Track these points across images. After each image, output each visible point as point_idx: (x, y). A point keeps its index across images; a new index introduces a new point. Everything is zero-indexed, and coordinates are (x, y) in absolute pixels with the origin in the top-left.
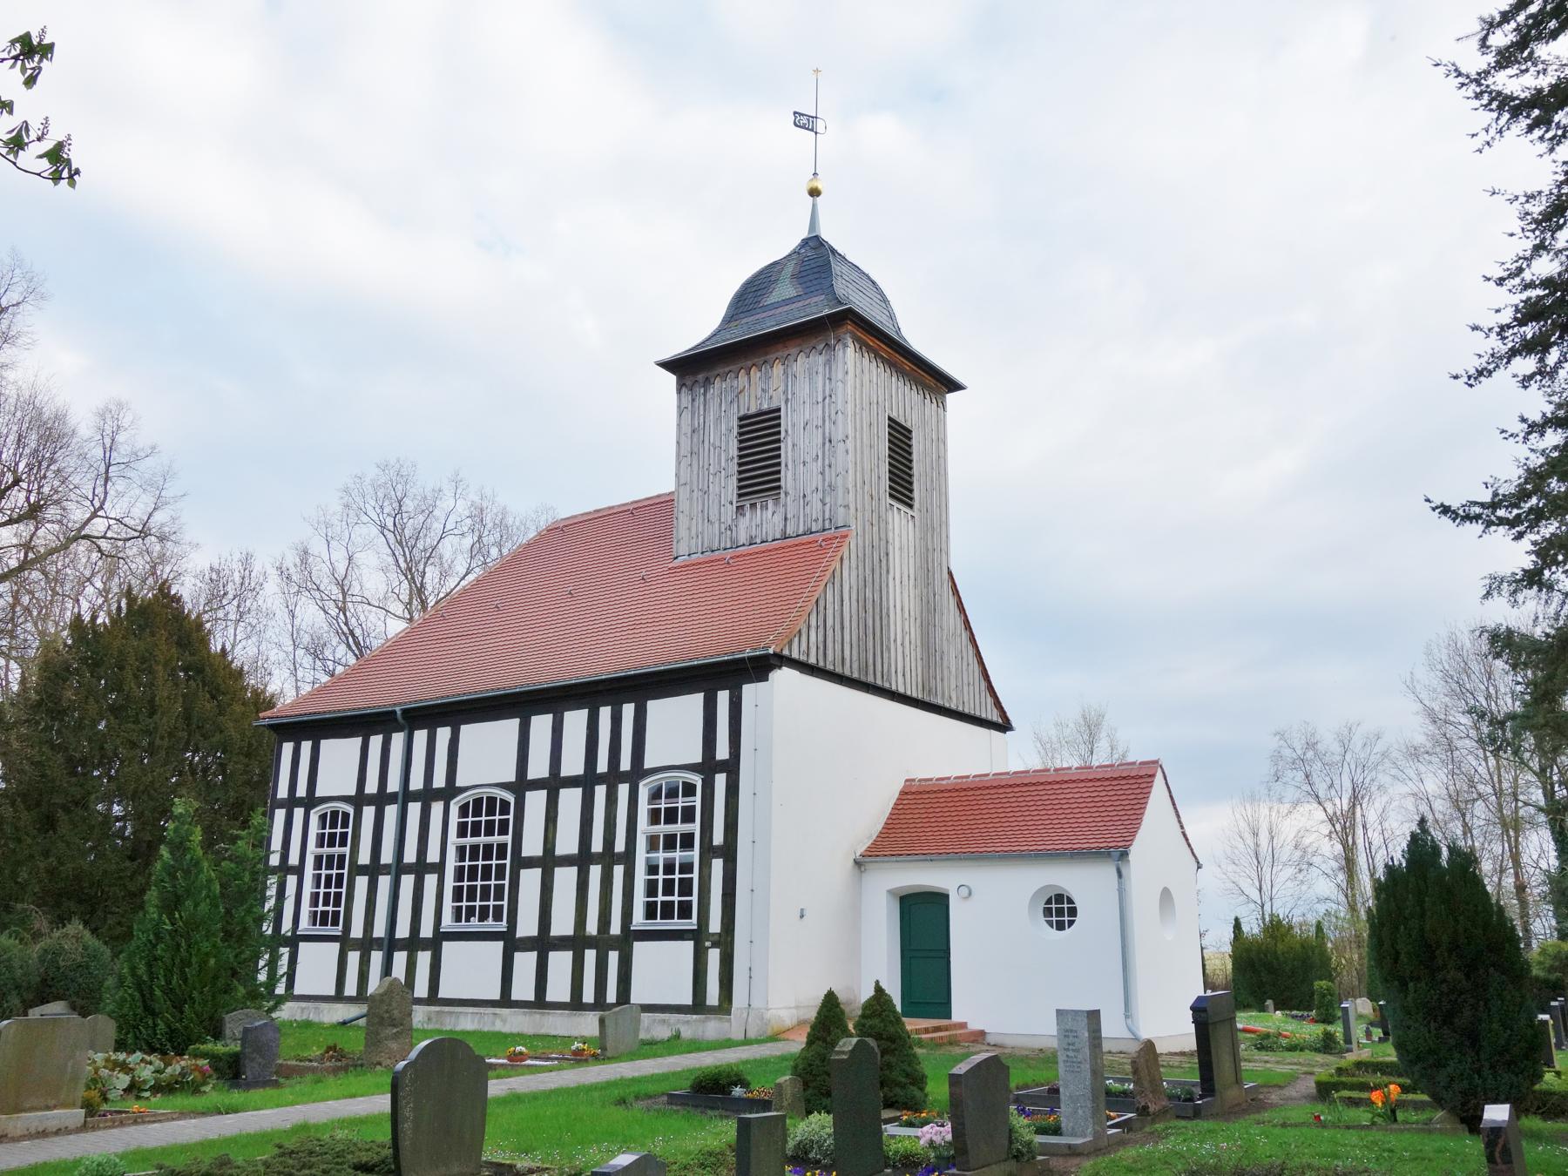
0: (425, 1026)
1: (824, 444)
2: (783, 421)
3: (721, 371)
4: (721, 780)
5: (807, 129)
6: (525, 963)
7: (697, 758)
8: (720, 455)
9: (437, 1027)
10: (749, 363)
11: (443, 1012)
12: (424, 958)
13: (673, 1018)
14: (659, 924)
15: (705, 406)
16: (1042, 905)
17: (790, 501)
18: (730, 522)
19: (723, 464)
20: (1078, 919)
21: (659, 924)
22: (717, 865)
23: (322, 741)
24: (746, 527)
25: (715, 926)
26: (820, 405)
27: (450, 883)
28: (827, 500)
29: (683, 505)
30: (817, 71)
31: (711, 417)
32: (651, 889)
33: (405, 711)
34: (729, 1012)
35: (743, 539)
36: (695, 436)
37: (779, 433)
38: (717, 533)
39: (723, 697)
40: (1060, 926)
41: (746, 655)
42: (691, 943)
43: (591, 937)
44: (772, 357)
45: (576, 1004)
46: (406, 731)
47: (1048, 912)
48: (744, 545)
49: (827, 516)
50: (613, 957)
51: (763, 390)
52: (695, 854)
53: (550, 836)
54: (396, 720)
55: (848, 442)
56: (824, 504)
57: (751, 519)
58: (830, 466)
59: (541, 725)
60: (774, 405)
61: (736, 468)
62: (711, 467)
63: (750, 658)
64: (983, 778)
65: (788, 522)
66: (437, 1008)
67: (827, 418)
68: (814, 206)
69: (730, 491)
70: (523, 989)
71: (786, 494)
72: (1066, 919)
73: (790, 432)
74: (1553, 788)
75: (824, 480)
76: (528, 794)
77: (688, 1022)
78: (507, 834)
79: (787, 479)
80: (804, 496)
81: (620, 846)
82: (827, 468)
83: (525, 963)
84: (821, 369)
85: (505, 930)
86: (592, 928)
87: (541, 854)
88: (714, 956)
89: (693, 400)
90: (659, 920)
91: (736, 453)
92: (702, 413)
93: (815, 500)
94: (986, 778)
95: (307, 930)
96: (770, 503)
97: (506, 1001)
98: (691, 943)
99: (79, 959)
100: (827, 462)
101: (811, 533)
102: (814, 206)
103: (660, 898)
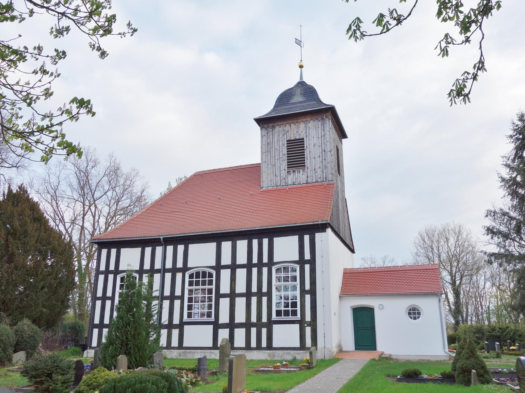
0: (178, 357)
1: (322, 152)
2: (305, 143)
3: (279, 124)
4: (307, 267)
5: (299, 45)
7: (214, 264)
8: (279, 153)
9: (184, 358)
10: (291, 122)
11: (187, 352)
12: (175, 332)
13: (292, 352)
14: (283, 318)
15: (272, 135)
16: (408, 312)
17: (309, 171)
18: (284, 176)
19: (281, 156)
21: (283, 318)
22: (308, 297)
23: (121, 249)
24: (291, 179)
25: (308, 318)
26: (320, 139)
27: (186, 303)
28: (324, 171)
29: (264, 168)
30: (301, 26)
31: (276, 139)
33: (164, 238)
35: (290, 182)
36: (269, 146)
37: (304, 147)
38: (279, 180)
39: (307, 238)
41: (319, 223)
42: (298, 325)
43: (254, 323)
44: (299, 120)
45: (259, 347)
46: (164, 246)
47: (409, 314)
48: (290, 185)
49: (324, 177)
50: (264, 331)
51: (296, 132)
52: (298, 293)
54: (160, 241)
55: (332, 152)
57: (293, 176)
58: (325, 160)
60: (301, 137)
61: (286, 158)
62: (276, 157)
63: (321, 224)
64: (374, 269)
65: (309, 178)
66: (183, 351)
67: (323, 143)
68: (301, 71)
69: (284, 166)
71: (307, 168)
73: (308, 147)
74: (94, 283)
75: (323, 164)
76: (222, 271)
77: (299, 353)
78: (212, 285)
79: (307, 163)
80: (315, 169)
81: (265, 289)
82: (324, 160)
84: (320, 126)
85: (214, 321)
86: (254, 319)
87: (229, 293)
88: (308, 330)
89: (267, 133)
90: (283, 317)
91: (286, 153)
92: (271, 137)
93: (319, 171)
94: (375, 269)
96: (301, 171)
98: (298, 325)
99: (31, 334)
100: (323, 158)
101: (318, 182)
102: (301, 71)
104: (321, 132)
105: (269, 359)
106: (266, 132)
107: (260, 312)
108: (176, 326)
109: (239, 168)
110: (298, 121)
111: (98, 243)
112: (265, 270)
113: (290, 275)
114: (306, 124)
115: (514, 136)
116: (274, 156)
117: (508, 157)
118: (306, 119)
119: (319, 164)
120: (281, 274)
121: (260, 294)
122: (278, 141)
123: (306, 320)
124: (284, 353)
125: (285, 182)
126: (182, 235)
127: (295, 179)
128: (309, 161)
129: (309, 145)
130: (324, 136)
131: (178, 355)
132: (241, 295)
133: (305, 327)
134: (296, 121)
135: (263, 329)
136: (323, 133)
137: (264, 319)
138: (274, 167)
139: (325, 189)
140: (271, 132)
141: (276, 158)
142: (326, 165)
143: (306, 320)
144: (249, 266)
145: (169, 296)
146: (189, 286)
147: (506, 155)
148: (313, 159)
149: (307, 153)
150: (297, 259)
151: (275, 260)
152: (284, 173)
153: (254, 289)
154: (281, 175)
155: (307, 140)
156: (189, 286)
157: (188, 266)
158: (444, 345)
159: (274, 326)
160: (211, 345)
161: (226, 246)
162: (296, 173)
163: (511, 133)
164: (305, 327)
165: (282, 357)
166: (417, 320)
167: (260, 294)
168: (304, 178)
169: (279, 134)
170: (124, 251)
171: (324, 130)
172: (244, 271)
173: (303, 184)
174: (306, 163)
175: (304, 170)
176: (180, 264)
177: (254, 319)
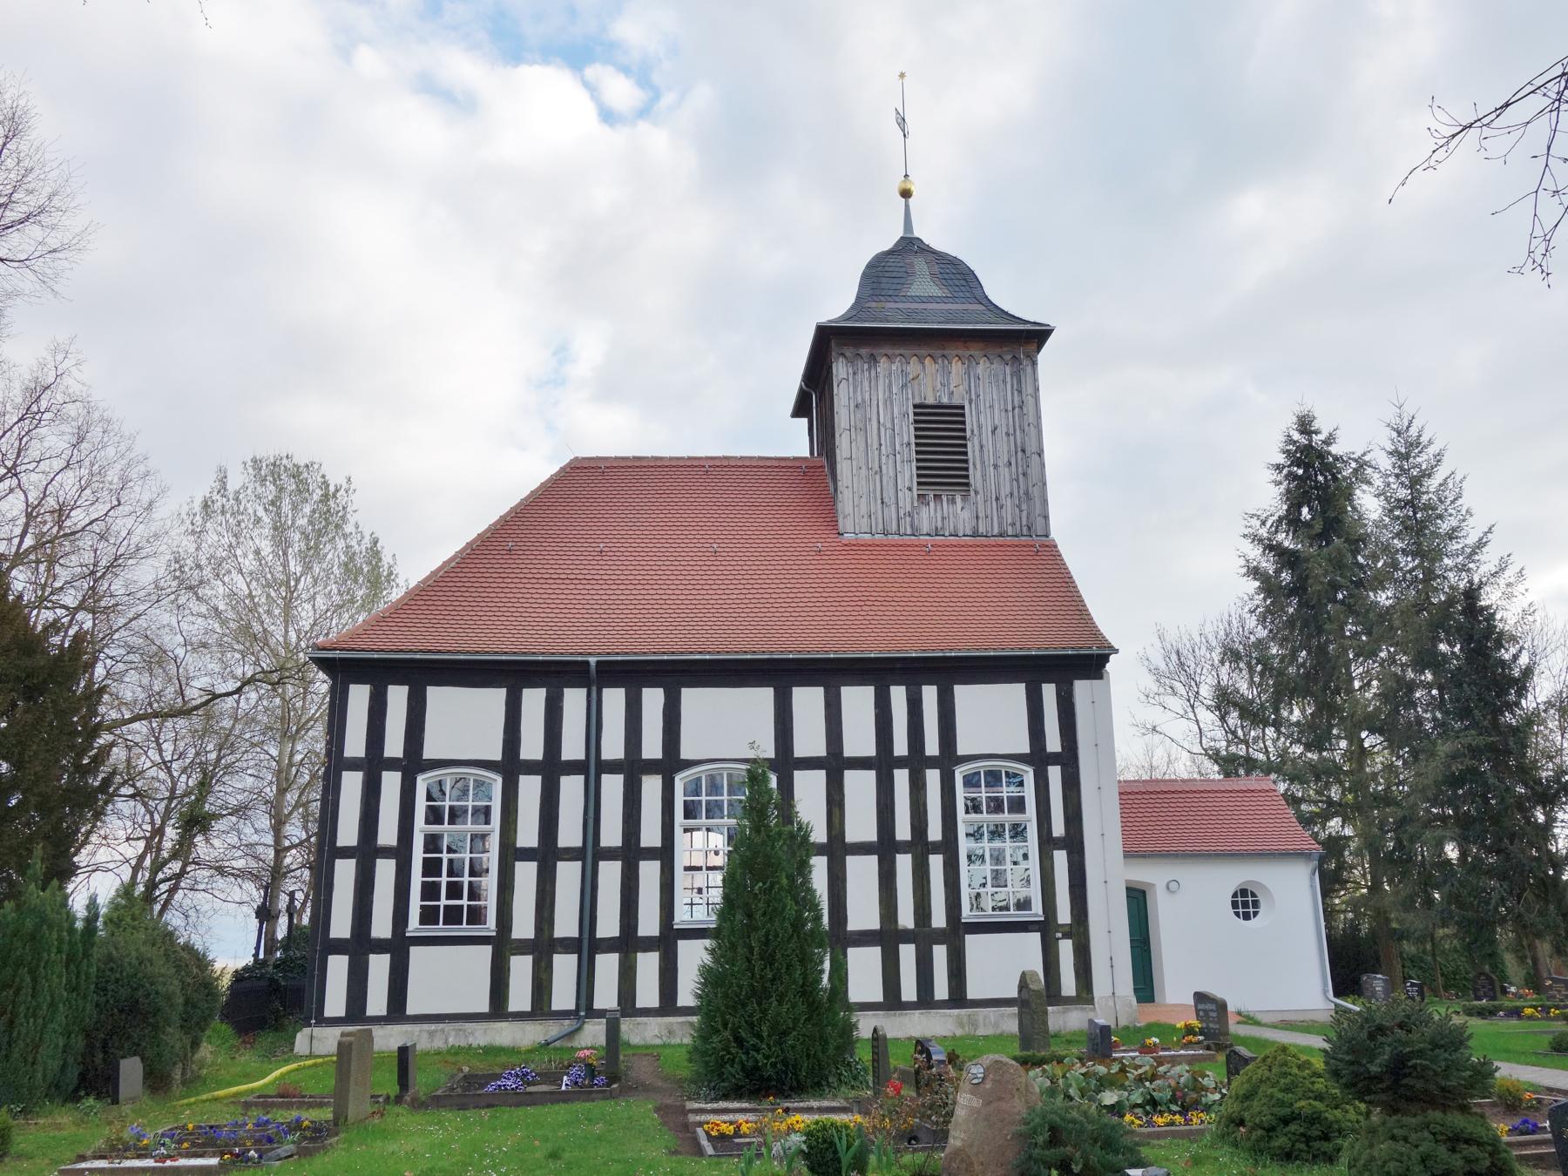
1: (1016, 453)
3: (890, 352)
4: (1055, 773)
6: (521, 968)
7: (1024, 748)
14: (441, 929)
18: (908, 508)
20: (1230, 899)
21: (441, 929)
22: (1060, 858)
24: (928, 517)
25: (1064, 916)
26: (1010, 414)
28: (1024, 507)
32: (430, 891)
34: (1091, 1001)
38: (894, 516)
39: (1049, 692)
40: (1247, 917)
44: (949, 352)
45: (926, 999)
49: (1024, 523)
50: (940, 953)
53: (836, 821)
56: (1021, 511)
59: (534, 700)
60: (956, 401)
62: (883, 447)
65: (980, 521)
68: (907, 206)
70: (520, 996)
71: (976, 492)
72: (1251, 910)
73: (976, 432)
75: (1019, 487)
79: (975, 476)
80: (997, 499)
81: (935, 833)
82: (1021, 477)
83: (521, 968)
84: (1008, 379)
85: (494, 934)
86: (906, 919)
88: (1066, 948)
89: (854, 374)
95: (417, 930)
96: (958, 499)
97: (498, 1007)
102: (907, 206)
103: (444, 902)
104: (1013, 394)
105: (959, 1032)
106: (851, 371)
107: (923, 900)
108: (648, 944)
109: (630, 464)
110: (945, 352)
111: (325, 664)
112: (933, 777)
113: (1005, 795)
114: (969, 367)
115: (1284, 467)
116: (876, 445)
117: (1263, 517)
118: (969, 353)
119: (1008, 484)
120: (978, 789)
121: (920, 847)
122: (889, 401)
123: (1060, 922)
124: (1002, 1015)
125: (912, 527)
126: (504, 658)
127: (939, 519)
128: (979, 474)
129: (980, 427)
130: (1021, 407)
131: (665, 1032)
132: (862, 849)
133: (1058, 939)
134: (939, 352)
135: (935, 948)
136: (1016, 399)
137: (939, 920)
138: (878, 477)
139: (508, 557)
140: (866, 374)
141: (883, 451)
142: (1028, 491)
143: (1060, 922)
144: (883, 763)
145: (618, 848)
146: (685, 818)
147: (1259, 513)
148: (992, 468)
149: (972, 449)
150: (1026, 749)
151: (962, 749)
152: (907, 500)
153: (903, 832)
154: (901, 504)
155: (974, 413)
156: (685, 818)
157: (683, 757)
158: (1325, 984)
159: (969, 939)
160: (484, 1007)
161: (534, 700)
162: (945, 503)
163: (1281, 459)
164: (1058, 939)
165: (996, 1025)
166: (1253, 922)
167: (920, 847)
168: (967, 520)
169: (890, 382)
170: (439, 698)
171: (1020, 392)
172: (870, 777)
173: (964, 536)
174: (971, 477)
175: (965, 498)
176: (652, 748)
177: (906, 919)
